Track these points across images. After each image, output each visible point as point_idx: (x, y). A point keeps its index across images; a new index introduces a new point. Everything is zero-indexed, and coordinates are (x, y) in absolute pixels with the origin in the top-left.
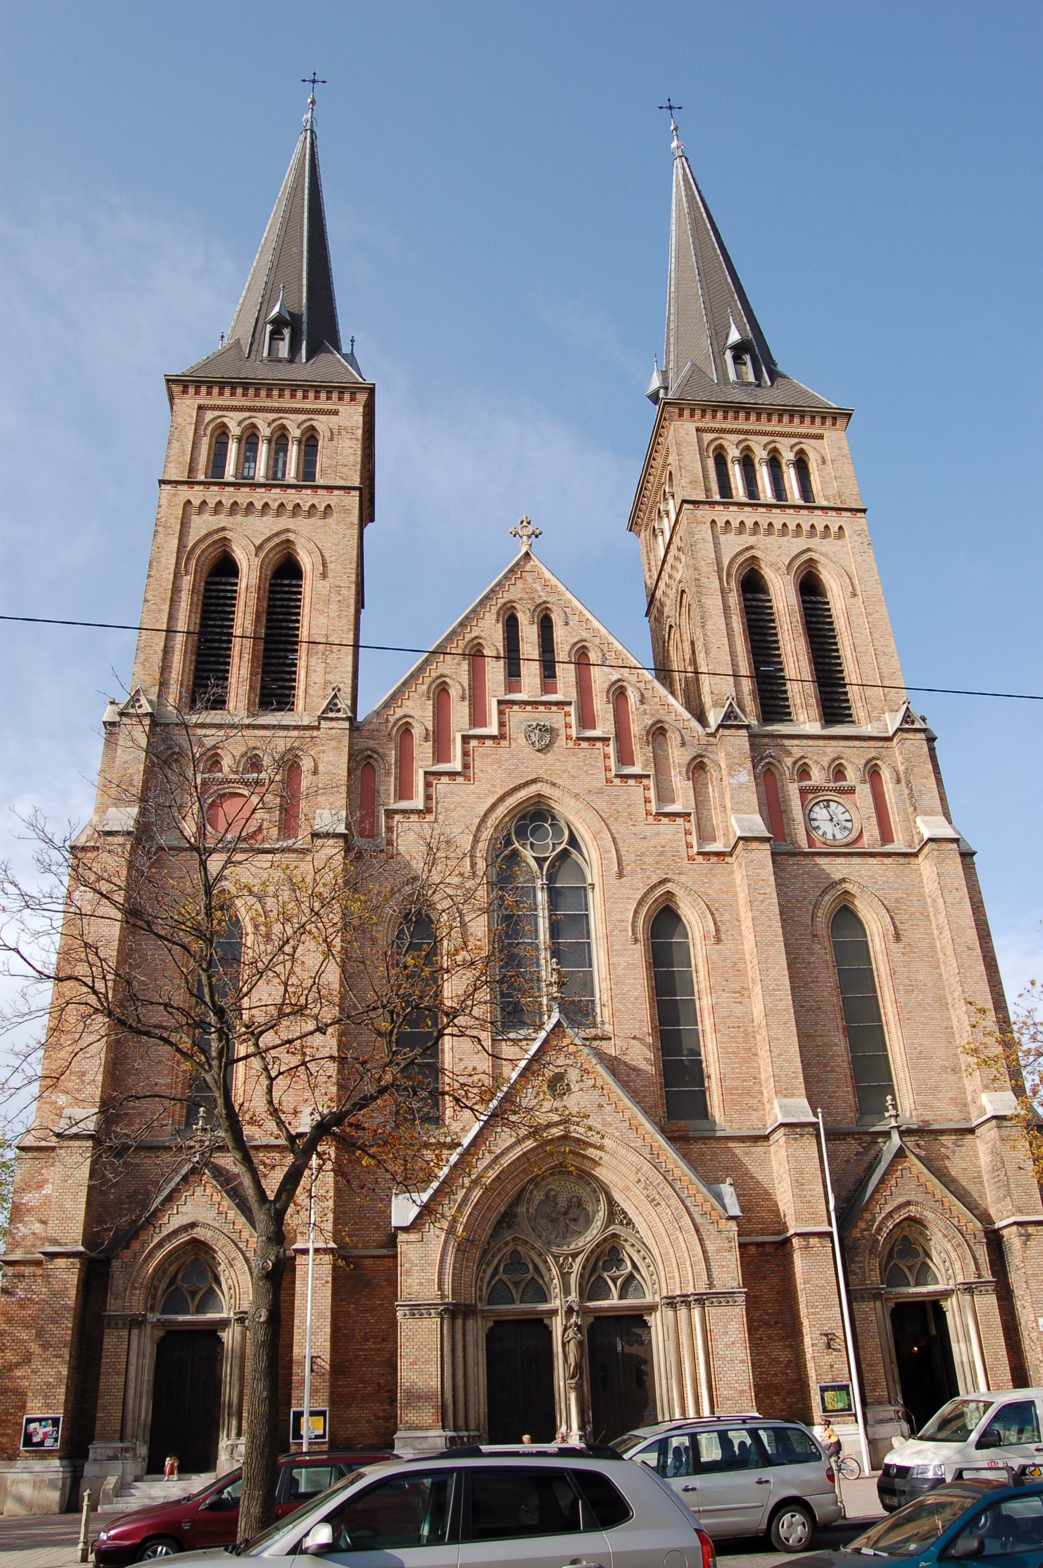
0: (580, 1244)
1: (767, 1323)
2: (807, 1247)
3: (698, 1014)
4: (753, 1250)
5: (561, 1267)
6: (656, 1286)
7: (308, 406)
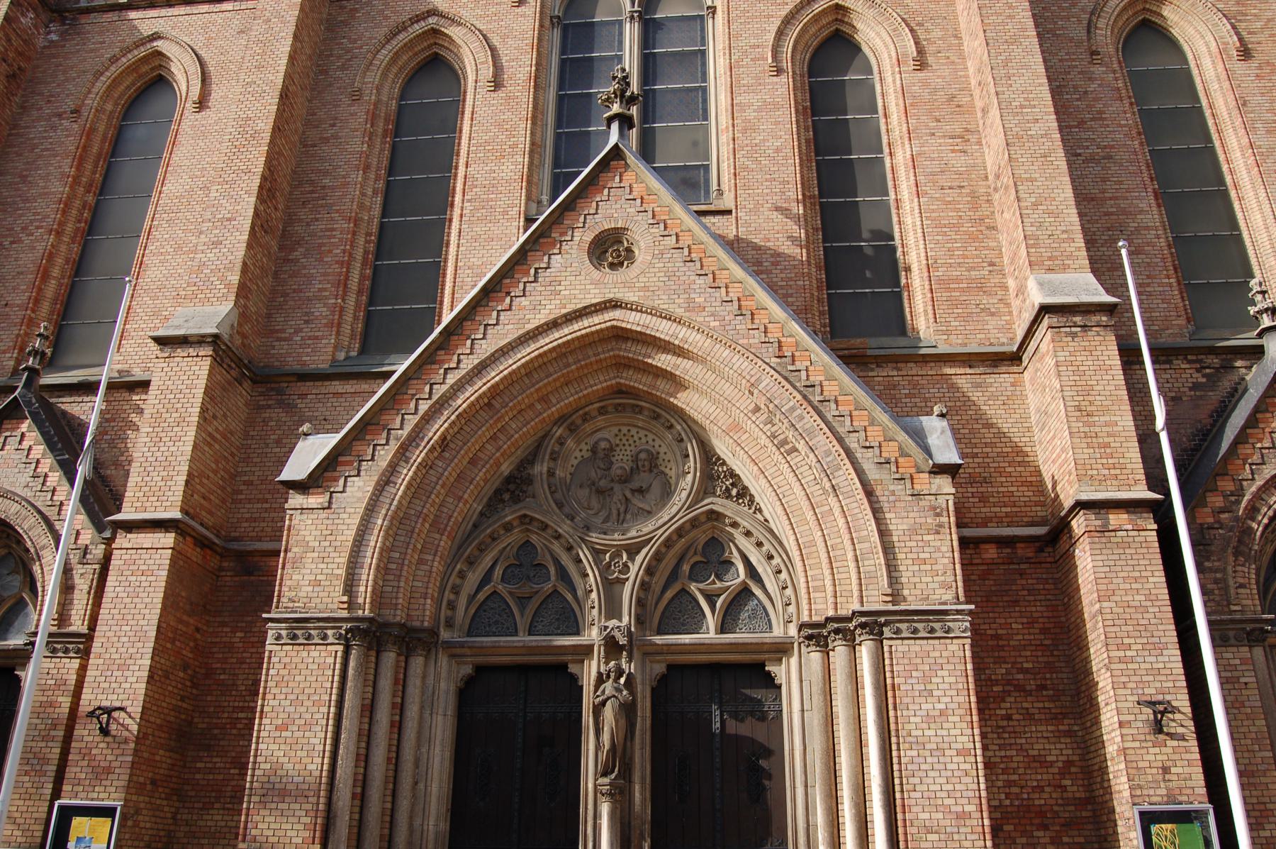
0: (645, 530)
1: (1020, 688)
2: (1104, 531)
3: (889, 176)
4: (991, 552)
5: (605, 570)
6: (792, 609)
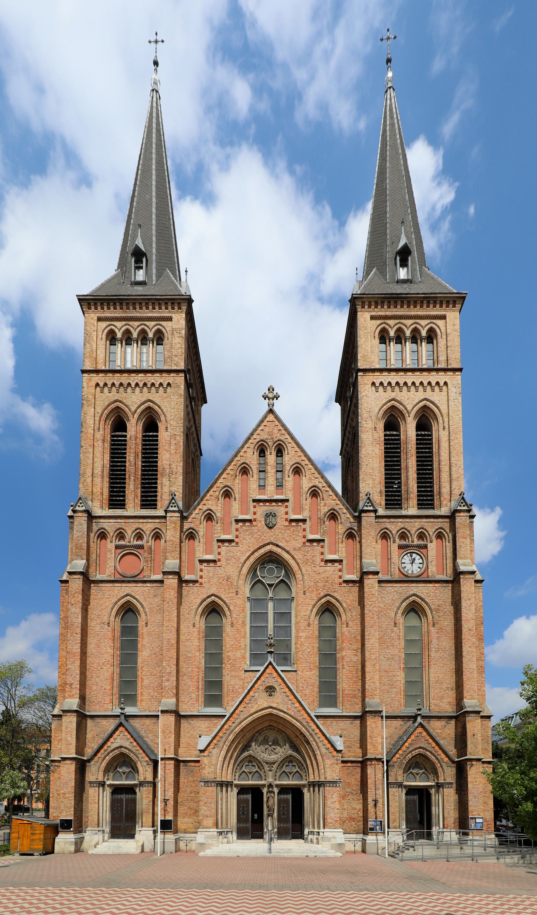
1: (352, 794)
7: (155, 315)
